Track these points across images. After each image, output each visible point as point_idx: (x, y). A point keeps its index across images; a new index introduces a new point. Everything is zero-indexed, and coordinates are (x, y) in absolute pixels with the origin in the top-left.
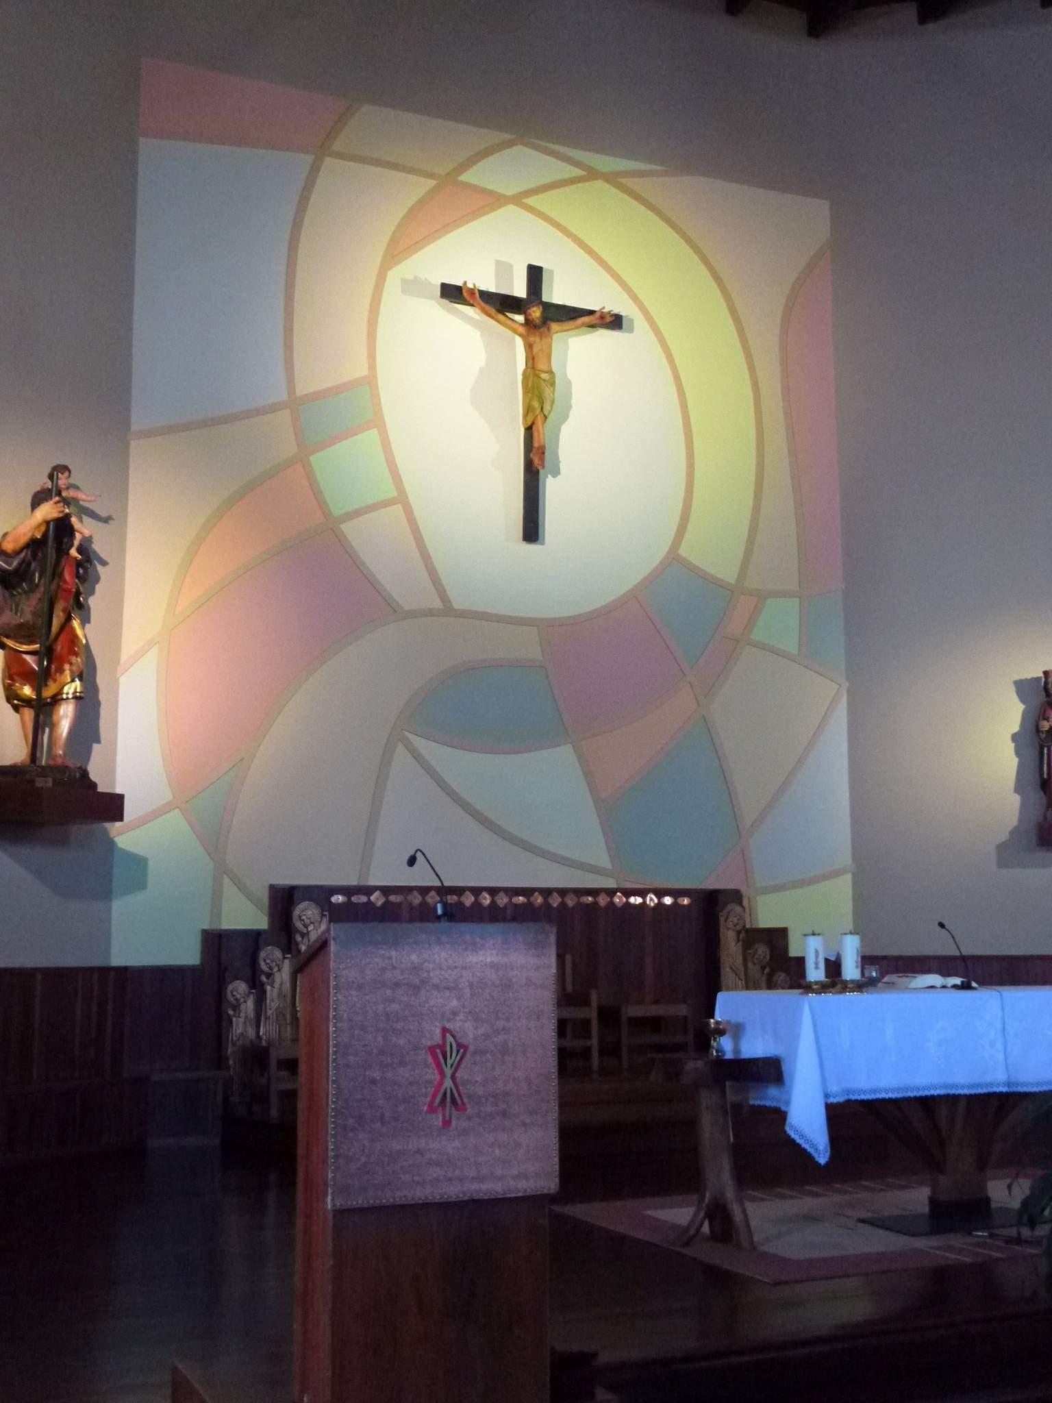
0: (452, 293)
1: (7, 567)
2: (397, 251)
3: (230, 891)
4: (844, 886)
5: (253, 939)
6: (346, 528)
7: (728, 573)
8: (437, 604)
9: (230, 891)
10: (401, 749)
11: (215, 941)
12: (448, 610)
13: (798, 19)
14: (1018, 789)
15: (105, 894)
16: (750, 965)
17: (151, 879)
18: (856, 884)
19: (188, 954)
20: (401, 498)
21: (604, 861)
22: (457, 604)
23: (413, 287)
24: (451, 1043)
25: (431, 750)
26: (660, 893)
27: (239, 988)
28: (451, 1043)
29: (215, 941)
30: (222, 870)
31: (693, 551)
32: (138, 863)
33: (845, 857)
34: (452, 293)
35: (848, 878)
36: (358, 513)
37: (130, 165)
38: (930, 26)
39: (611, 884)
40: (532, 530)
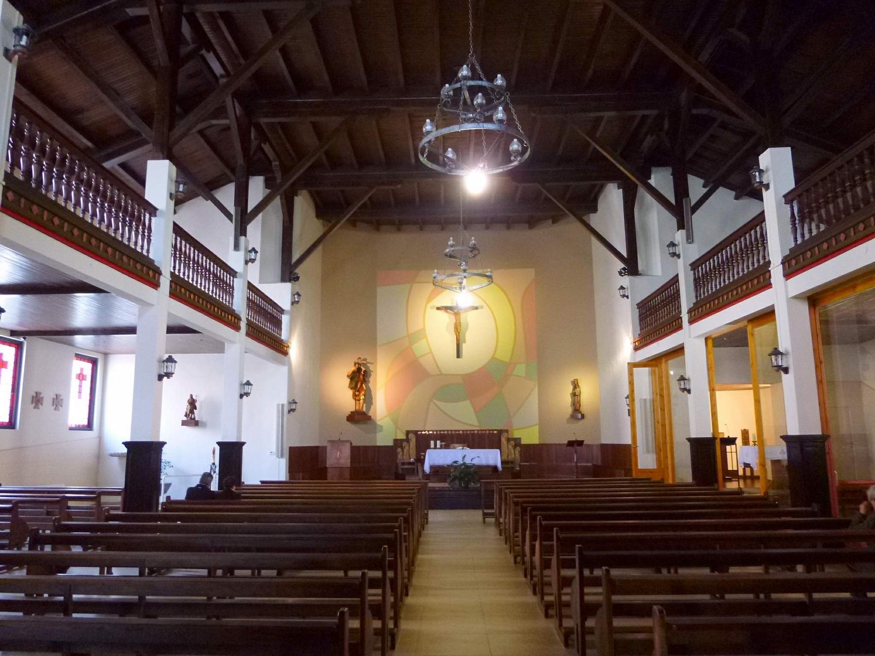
0: (438, 308)
1: (529, 149)
2: (431, 298)
3: (398, 431)
4: (537, 427)
5: (402, 441)
6: (420, 360)
7: (508, 360)
8: (439, 373)
9: (398, 431)
10: (432, 403)
11: (396, 441)
12: (441, 374)
13: (527, 225)
14: (571, 406)
15: (375, 433)
16: (509, 446)
17: (384, 429)
18: (539, 429)
19: (391, 443)
20: (431, 352)
21: (476, 423)
22: (443, 373)
23: (432, 308)
24: (80, 397)
25: (438, 403)
26: (433, 431)
27: (399, 450)
28: (80, 397)
29: (396, 441)
30: (397, 428)
31: (497, 356)
32: (381, 427)
33: (537, 421)
34: (438, 308)
35: (537, 426)
36: (422, 356)
37: (374, 297)
38: (555, 225)
39: (478, 429)
40: (458, 356)
